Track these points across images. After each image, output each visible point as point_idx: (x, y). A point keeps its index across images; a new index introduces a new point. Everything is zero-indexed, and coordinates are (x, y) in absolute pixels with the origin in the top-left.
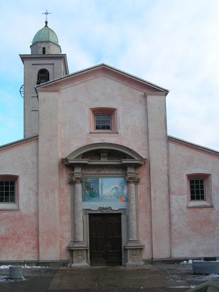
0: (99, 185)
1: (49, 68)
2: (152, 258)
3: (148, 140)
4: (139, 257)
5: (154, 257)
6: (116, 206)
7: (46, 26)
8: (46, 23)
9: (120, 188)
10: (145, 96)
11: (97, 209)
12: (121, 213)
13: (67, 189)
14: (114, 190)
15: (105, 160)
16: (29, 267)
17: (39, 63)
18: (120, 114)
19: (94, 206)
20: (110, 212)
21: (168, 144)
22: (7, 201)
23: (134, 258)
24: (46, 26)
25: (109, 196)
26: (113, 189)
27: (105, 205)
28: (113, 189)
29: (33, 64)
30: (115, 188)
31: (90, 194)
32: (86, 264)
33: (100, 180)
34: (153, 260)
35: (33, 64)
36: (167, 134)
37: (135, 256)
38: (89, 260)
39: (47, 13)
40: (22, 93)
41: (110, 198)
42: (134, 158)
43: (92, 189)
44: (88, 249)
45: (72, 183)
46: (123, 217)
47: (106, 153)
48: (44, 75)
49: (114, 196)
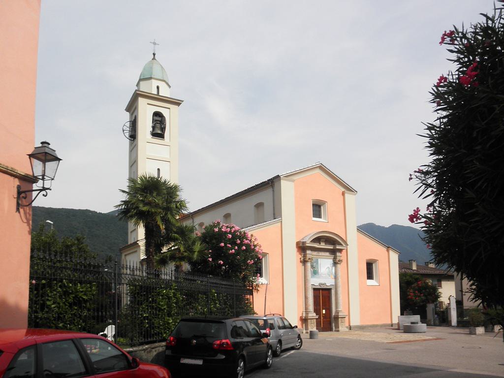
3: (274, 214)
6: (329, 282)
7: (154, 59)
8: (154, 54)
10: (343, 194)
11: (317, 285)
12: (331, 289)
13: (302, 268)
17: (155, 104)
19: (315, 282)
20: (325, 287)
21: (30, 159)
23: (312, 326)
24: (154, 59)
29: (148, 104)
32: (26, 358)
33: (319, 260)
35: (148, 104)
39: (155, 44)
40: (125, 132)
45: (304, 262)
46: (333, 292)
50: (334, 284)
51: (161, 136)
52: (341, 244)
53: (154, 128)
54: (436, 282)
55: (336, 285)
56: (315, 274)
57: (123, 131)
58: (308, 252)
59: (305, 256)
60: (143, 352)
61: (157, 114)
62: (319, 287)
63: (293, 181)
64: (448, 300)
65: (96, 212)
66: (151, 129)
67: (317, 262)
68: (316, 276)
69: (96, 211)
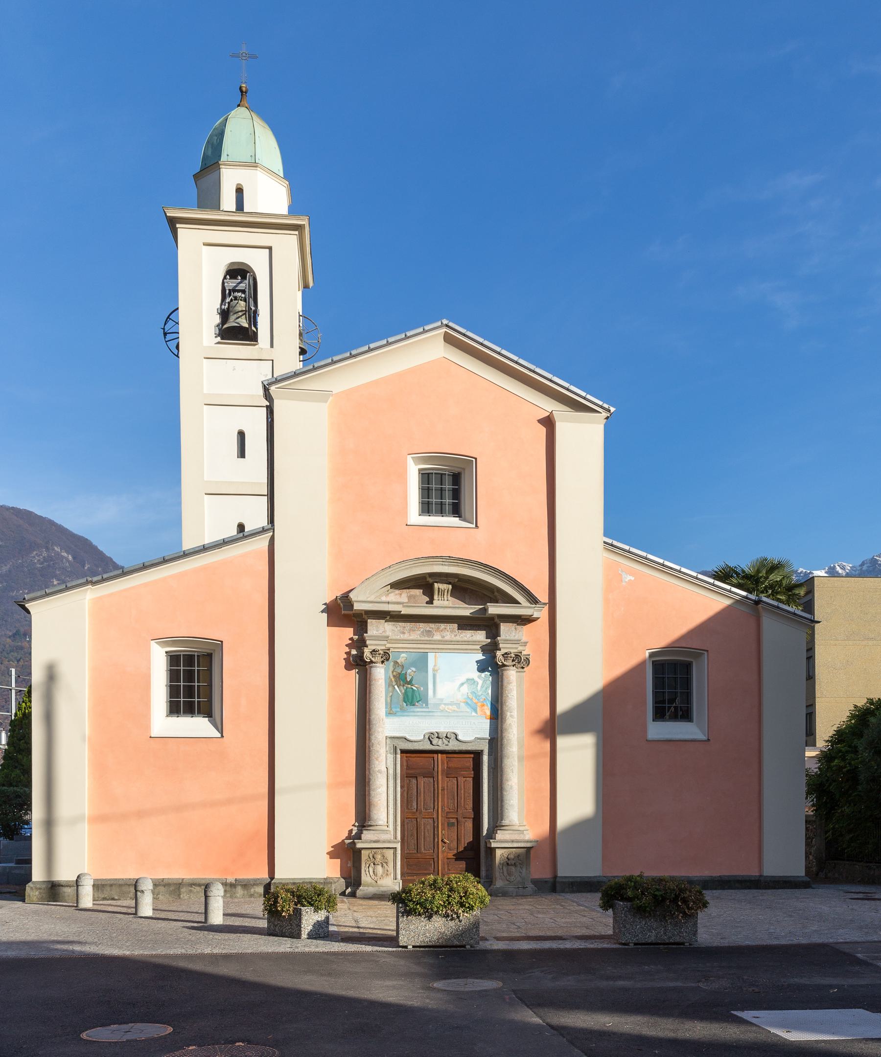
0: (427, 672)
1: (257, 261)
2: (555, 877)
4: (524, 870)
5: (560, 873)
9: (480, 682)
14: (465, 686)
15: (446, 603)
16: (532, 1018)
18: (482, 468)
20: (453, 746)
22: (173, 691)
25: (452, 704)
26: (462, 684)
27: (442, 726)
28: (462, 684)
30: (468, 680)
31: (405, 695)
33: (431, 656)
34: (558, 879)
36: (802, 876)
37: (513, 868)
38: (399, 876)
40: (169, 337)
41: (454, 708)
42: (519, 603)
43: (410, 683)
44: (398, 846)
47: (449, 583)
48: (242, 286)
49: (467, 703)
50: (487, 735)
51: (247, 335)
52: (514, 601)
53: (225, 315)
54: (451, 765)
55: (496, 741)
56: (413, 704)
57: (165, 334)
58: (375, 628)
59: (360, 643)
60: (116, 898)
61: (238, 272)
62: (429, 747)
63: (322, 396)
64: (131, 886)
65: (92, 543)
66: (217, 319)
67: (421, 662)
68: (412, 708)
69: (92, 541)
